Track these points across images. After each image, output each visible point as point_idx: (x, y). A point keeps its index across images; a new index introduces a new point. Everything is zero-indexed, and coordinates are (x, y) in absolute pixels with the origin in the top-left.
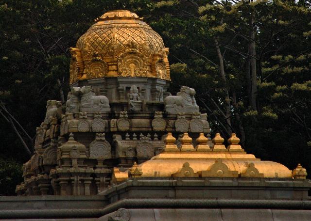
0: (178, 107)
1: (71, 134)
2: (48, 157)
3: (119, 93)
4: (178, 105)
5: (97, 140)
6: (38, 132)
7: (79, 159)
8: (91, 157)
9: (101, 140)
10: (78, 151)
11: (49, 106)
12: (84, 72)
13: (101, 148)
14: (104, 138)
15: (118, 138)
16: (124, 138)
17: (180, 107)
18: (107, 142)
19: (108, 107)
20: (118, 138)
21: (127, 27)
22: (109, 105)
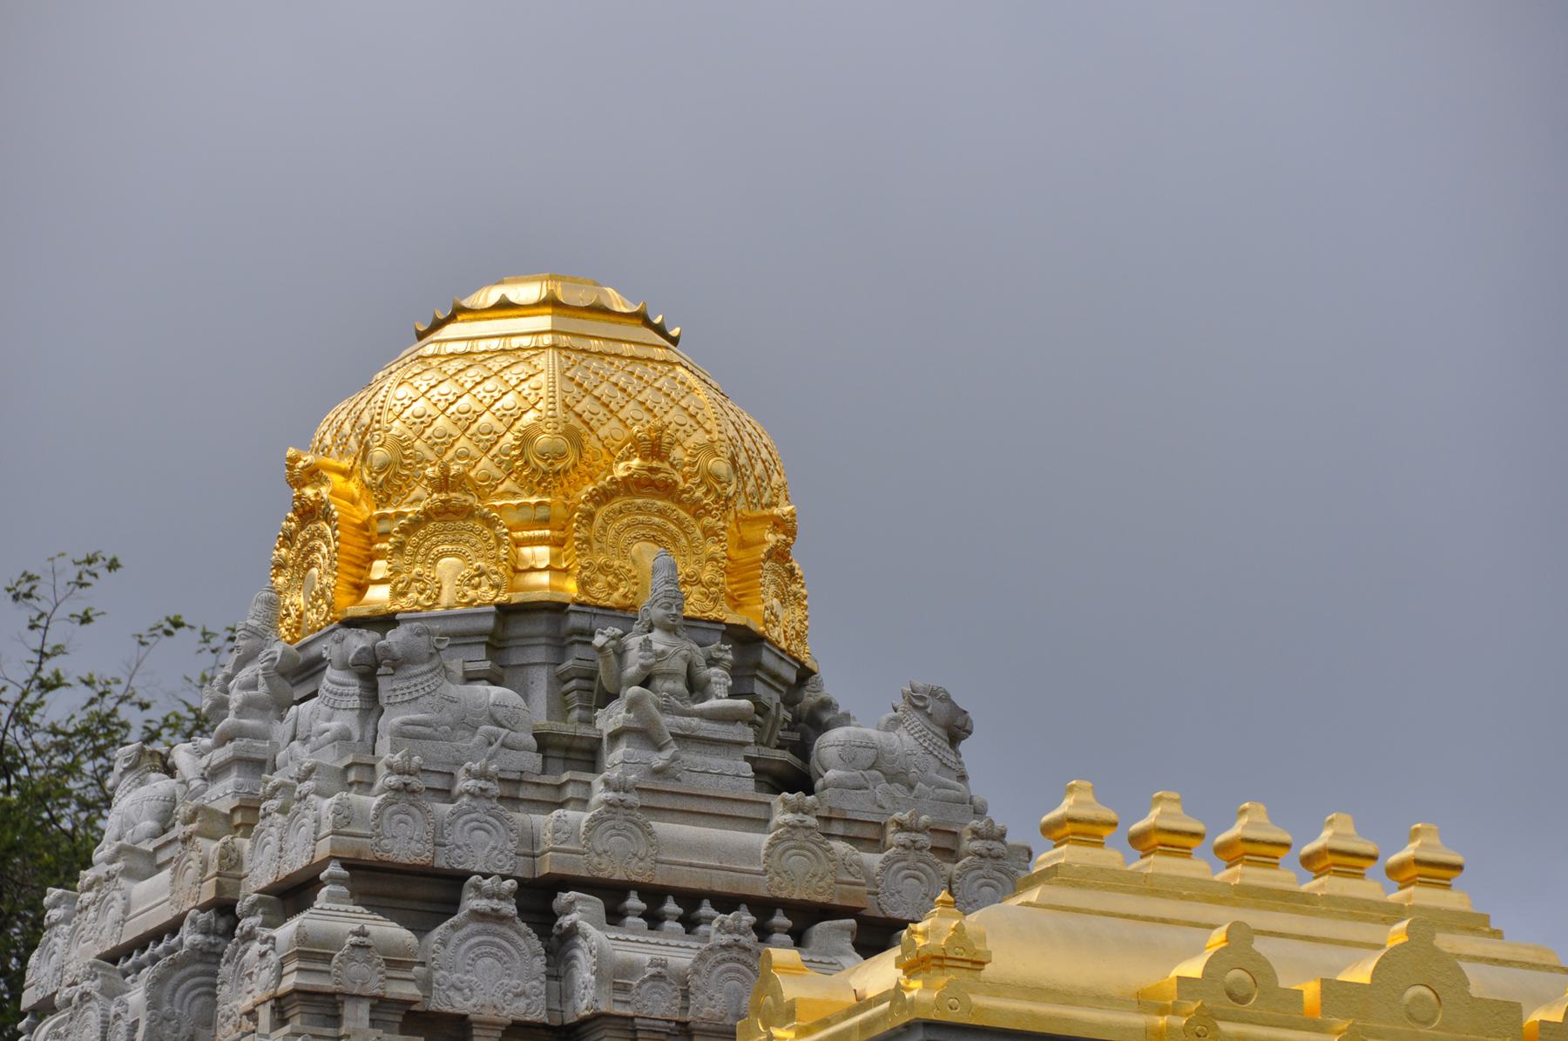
0: (891, 788)
1: (334, 869)
2: (166, 1008)
3: (566, 703)
4: (891, 778)
5: (479, 915)
6: (54, 914)
7: (380, 1004)
8: (438, 1003)
9: (497, 917)
10: (379, 958)
11: (129, 778)
12: (375, 576)
13: (488, 961)
14: (510, 908)
15: (581, 912)
16: (615, 916)
17: (898, 790)
18: (523, 926)
19: (527, 749)
20: (581, 912)
21: (652, 360)
22: (533, 742)
